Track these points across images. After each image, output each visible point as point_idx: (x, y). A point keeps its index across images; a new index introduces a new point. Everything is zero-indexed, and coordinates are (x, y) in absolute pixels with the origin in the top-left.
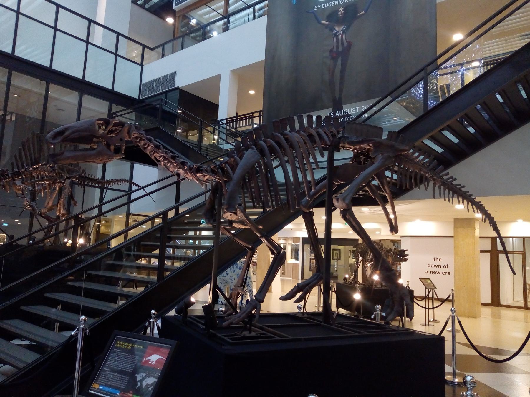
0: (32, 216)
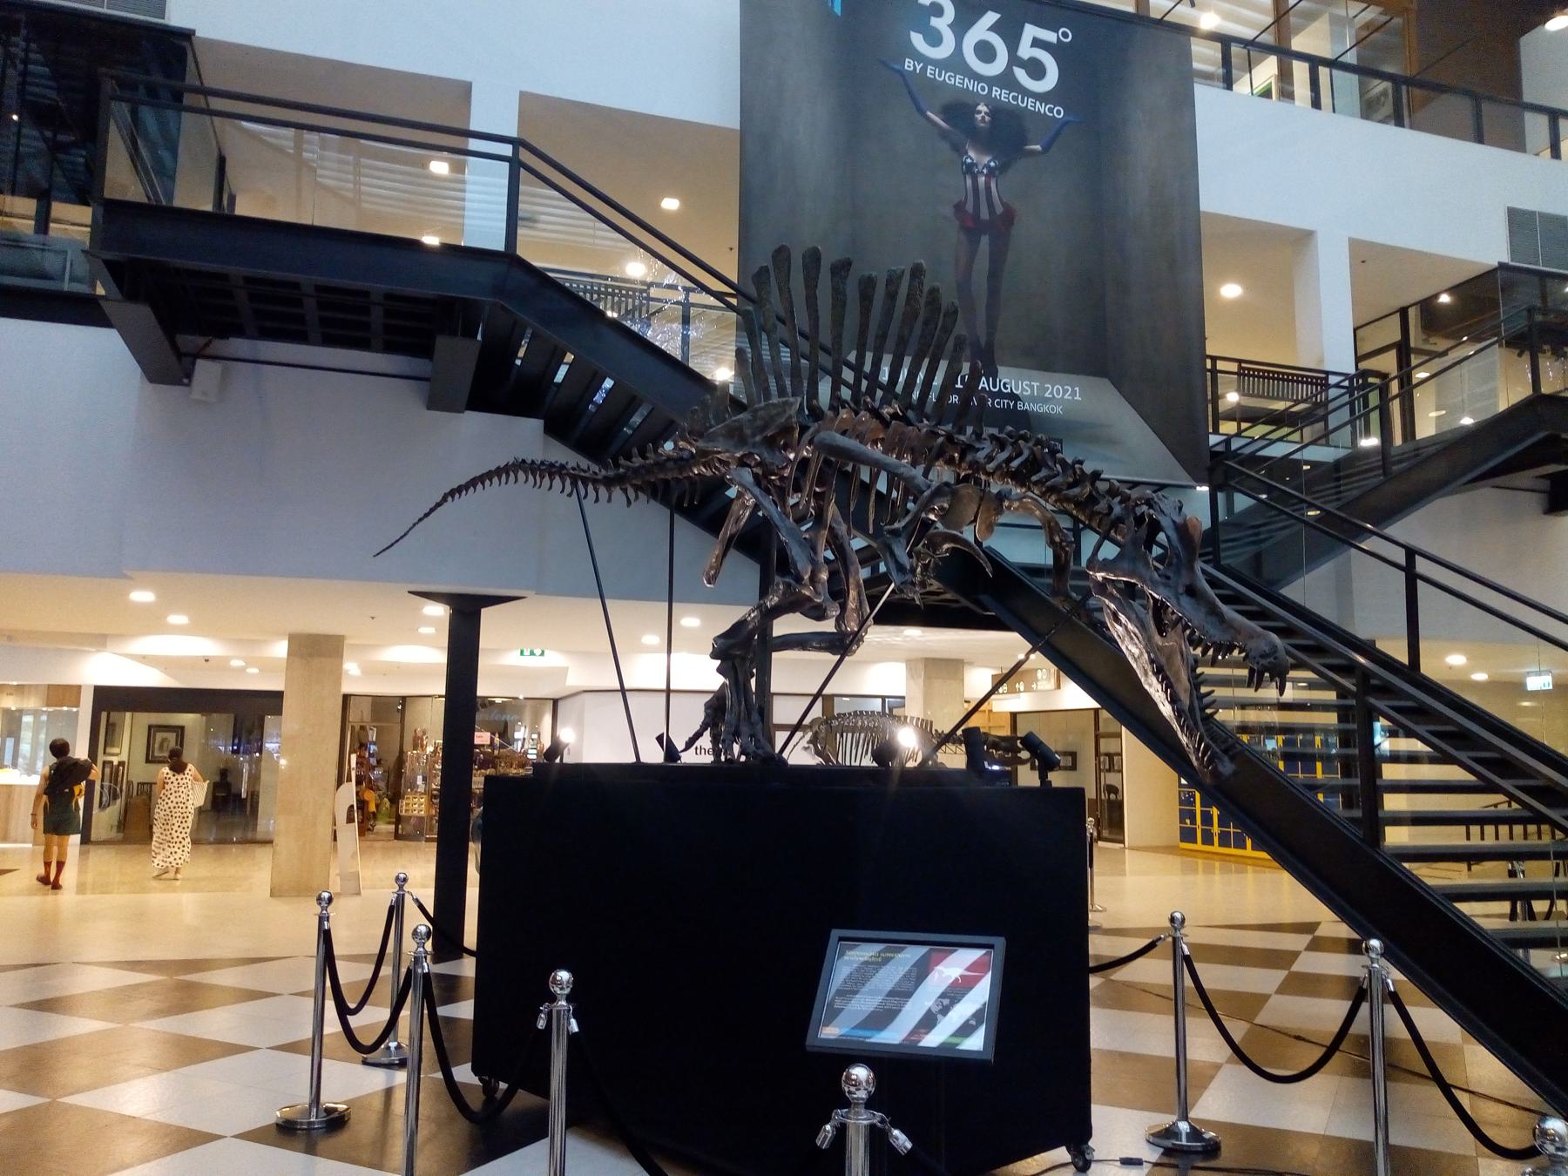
0: (686, 320)
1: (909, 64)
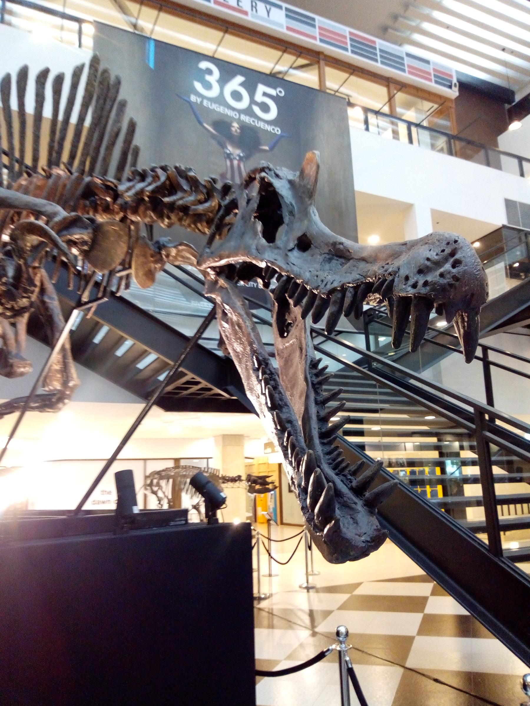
1: (193, 98)
